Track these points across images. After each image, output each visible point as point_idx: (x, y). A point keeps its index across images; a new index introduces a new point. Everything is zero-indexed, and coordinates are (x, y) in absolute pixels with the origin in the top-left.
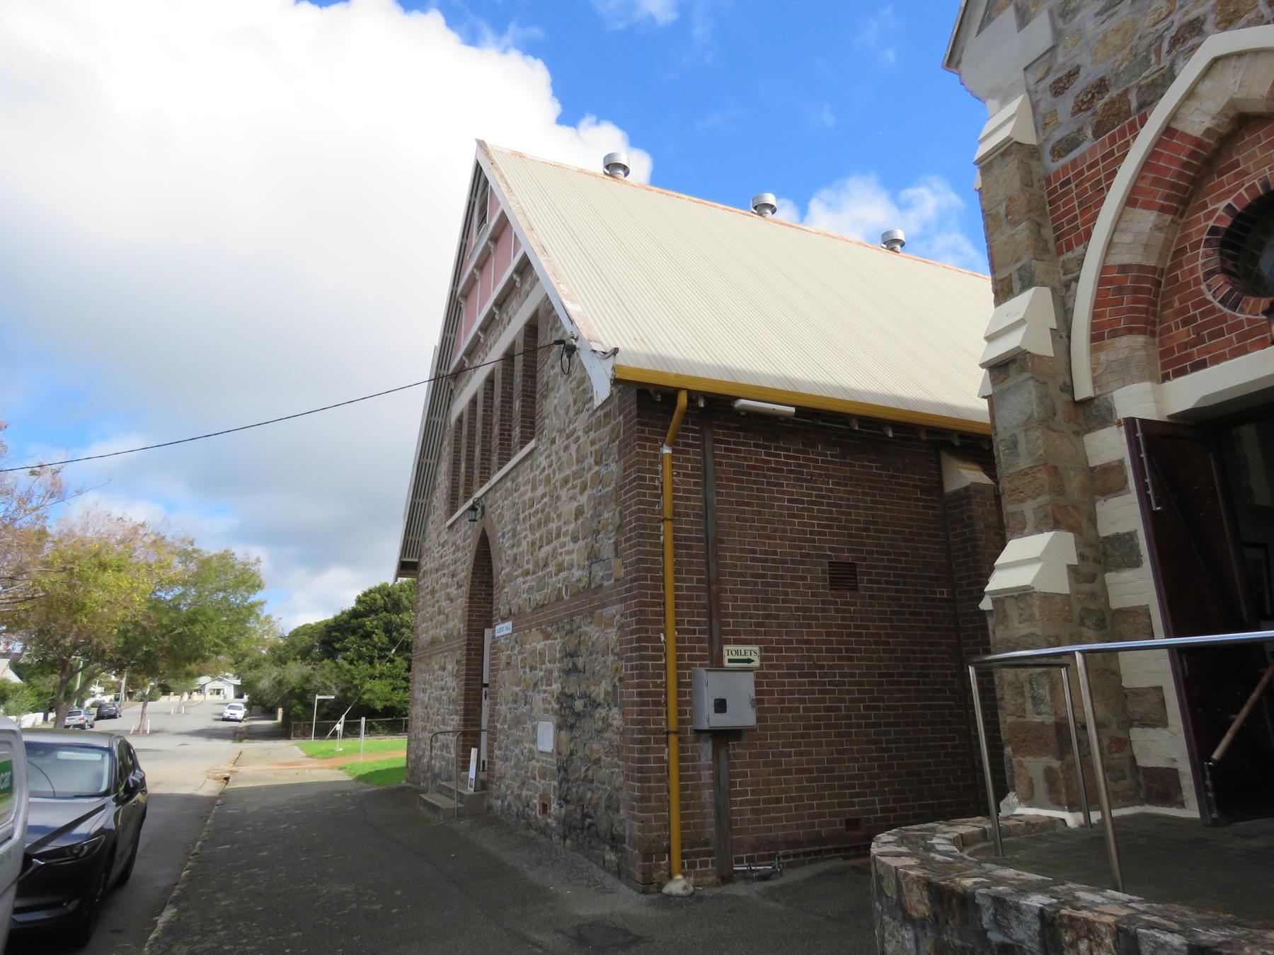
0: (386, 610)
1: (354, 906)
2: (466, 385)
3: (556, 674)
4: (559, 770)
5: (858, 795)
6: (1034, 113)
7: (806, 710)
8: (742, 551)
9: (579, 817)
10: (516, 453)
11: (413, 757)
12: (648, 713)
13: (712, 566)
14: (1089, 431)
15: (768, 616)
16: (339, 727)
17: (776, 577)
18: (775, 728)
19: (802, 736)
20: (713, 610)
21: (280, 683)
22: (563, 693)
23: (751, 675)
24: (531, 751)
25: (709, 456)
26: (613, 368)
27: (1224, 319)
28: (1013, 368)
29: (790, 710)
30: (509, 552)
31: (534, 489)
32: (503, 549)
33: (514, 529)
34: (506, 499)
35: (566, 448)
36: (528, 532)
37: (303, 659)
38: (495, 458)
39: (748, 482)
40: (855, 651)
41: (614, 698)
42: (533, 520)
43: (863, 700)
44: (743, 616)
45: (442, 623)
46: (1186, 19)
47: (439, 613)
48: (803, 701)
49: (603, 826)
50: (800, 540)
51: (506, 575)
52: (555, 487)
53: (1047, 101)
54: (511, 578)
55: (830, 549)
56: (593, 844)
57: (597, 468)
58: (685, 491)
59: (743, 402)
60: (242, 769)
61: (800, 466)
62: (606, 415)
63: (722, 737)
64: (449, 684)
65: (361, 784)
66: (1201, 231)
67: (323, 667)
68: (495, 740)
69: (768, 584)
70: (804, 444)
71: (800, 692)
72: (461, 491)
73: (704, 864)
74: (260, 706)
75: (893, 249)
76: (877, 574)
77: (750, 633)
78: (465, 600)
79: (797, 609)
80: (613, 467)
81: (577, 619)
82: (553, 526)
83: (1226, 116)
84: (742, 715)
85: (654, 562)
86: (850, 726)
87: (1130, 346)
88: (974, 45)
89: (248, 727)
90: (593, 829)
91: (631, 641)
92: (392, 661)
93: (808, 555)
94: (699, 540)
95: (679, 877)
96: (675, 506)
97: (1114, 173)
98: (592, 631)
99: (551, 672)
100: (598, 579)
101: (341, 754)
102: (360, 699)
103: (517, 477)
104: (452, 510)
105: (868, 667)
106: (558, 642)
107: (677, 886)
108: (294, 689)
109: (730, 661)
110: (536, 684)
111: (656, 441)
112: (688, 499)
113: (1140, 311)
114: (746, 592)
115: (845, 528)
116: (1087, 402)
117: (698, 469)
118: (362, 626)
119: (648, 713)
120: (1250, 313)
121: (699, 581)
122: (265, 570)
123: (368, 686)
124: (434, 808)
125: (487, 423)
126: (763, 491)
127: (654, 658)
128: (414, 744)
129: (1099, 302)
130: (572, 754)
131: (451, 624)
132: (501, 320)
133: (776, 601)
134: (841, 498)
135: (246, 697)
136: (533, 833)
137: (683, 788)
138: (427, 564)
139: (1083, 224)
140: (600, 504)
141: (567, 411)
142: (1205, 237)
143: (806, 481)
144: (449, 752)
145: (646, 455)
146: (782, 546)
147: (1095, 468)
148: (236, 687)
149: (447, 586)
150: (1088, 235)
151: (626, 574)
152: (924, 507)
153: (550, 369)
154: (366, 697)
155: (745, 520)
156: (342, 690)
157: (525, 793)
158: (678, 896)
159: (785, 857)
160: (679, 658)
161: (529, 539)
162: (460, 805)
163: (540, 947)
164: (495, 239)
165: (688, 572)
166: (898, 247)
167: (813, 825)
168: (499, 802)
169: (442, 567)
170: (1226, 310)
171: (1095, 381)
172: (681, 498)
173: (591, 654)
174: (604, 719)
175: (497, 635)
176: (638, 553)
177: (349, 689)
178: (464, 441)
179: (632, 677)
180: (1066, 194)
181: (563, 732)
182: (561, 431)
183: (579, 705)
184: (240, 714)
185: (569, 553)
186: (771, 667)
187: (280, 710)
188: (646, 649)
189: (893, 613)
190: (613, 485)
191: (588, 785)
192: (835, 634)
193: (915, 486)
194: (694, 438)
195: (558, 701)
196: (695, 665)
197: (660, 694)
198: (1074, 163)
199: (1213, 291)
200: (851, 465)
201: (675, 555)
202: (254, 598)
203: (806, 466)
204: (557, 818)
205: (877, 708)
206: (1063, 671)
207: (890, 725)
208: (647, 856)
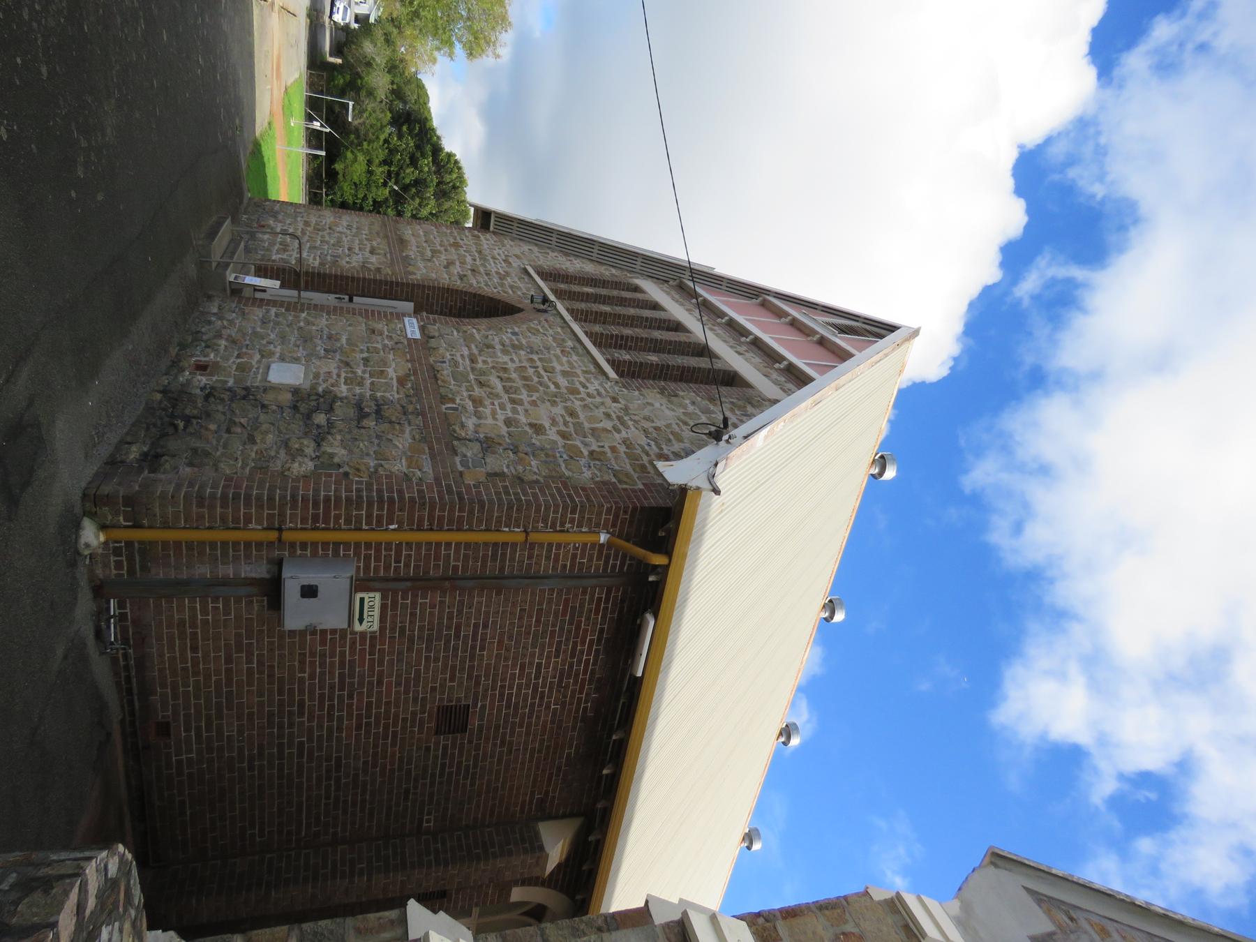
0: (439, 183)
1: (84, 144)
2: (673, 298)
3: (358, 390)
4: (246, 389)
5: (198, 735)
7: (302, 680)
8: (487, 613)
9: (187, 412)
10: (603, 354)
11: (277, 208)
12: (305, 508)
13: (471, 583)
15: (411, 640)
16: (316, 125)
17: (456, 649)
18: (281, 647)
19: (271, 676)
20: (422, 582)
21: (369, 64)
22: (335, 398)
23: (345, 626)
24: (272, 354)
25: (594, 581)
26: (698, 488)
29: (302, 663)
30: (497, 339)
31: (565, 374)
32: (498, 333)
33: (520, 347)
34: (554, 339)
35: (608, 416)
36: (518, 364)
37: (393, 92)
38: (597, 328)
39: (563, 621)
40: (368, 732)
41: (325, 463)
42: (531, 371)
43: (310, 740)
44: (413, 615)
45: (422, 254)
47: (433, 252)
48: (312, 677)
49: (172, 444)
50: (495, 675)
51: (472, 335)
52: (566, 400)
54: (468, 339)
55: (483, 707)
56: (153, 430)
57: (586, 453)
58: (557, 555)
59: (652, 623)
60: (275, 15)
61: (577, 675)
62: (643, 467)
63: (273, 590)
64: (355, 258)
65: (250, 147)
67: (383, 111)
68: (288, 310)
69: (448, 642)
70: (599, 680)
71: (322, 674)
72: (562, 286)
73: (119, 565)
74: (346, 39)
75: (781, 734)
76: (453, 754)
77: (393, 622)
78: (447, 282)
79: (418, 672)
80: (587, 474)
81: (419, 421)
82: (524, 395)
84: (297, 614)
85: (480, 521)
86: (281, 727)
88: (1013, 882)
89: (323, 26)
90: (171, 430)
91: (390, 490)
92: (385, 184)
93: (478, 683)
94: (502, 569)
95: (102, 538)
96: (541, 545)
98: (404, 440)
99: (361, 384)
100: (464, 450)
101: (287, 123)
102: (347, 148)
103: (577, 354)
104: (545, 275)
105: (348, 745)
106: (394, 395)
107: (91, 536)
108: (361, 78)
109: (362, 600)
110: (347, 364)
111: (614, 525)
112: (548, 558)
114: (441, 618)
115: (506, 722)
117: (580, 569)
118: (423, 155)
119: (305, 508)
121: (455, 568)
122: (487, 60)
123: (361, 157)
124: (213, 234)
125: (632, 321)
126: (552, 637)
127: (369, 516)
128: (291, 210)
130: (264, 406)
131: (421, 264)
132: (741, 344)
133: (428, 649)
134: (538, 717)
135: (356, 26)
136: (174, 351)
137: (213, 545)
138: (487, 240)
140: (547, 455)
141: (647, 419)
143: (561, 681)
144: (278, 253)
145: (599, 514)
146: (490, 657)
148: (368, 16)
149: (463, 263)
151: (468, 487)
152: (524, 802)
153: (691, 403)
154: (349, 155)
155: (521, 618)
156: (357, 130)
157: (223, 343)
158: (78, 537)
159: (125, 656)
160: (368, 545)
161: (511, 366)
162: (214, 265)
163: (7, 381)
164: (822, 342)
165: (466, 556)
166: (783, 739)
167: (163, 686)
168: (215, 310)
169: (483, 258)
172: (549, 550)
173: (378, 437)
174: (300, 451)
175: (406, 319)
176: (491, 502)
177: (358, 137)
178: (615, 293)
179: (349, 490)
181: (289, 396)
182: (626, 409)
183: (320, 419)
184: (338, 17)
185: (494, 413)
186: (353, 643)
187: (339, 61)
188: (381, 508)
189: (409, 772)
190: (567, 473)
191: (224, 427)
192: (387, 711)
193: (547, 793)
194: (614, 566)
195: (327, 392)
196: (359, 561)
197: (326, 521)
200: (574, 728)
201: (486, 544)
202: (458, 48)
203: (576, 682)
204: (189, 382)
205: (301, 755)
207: (281, 769)
208: (129, 501)
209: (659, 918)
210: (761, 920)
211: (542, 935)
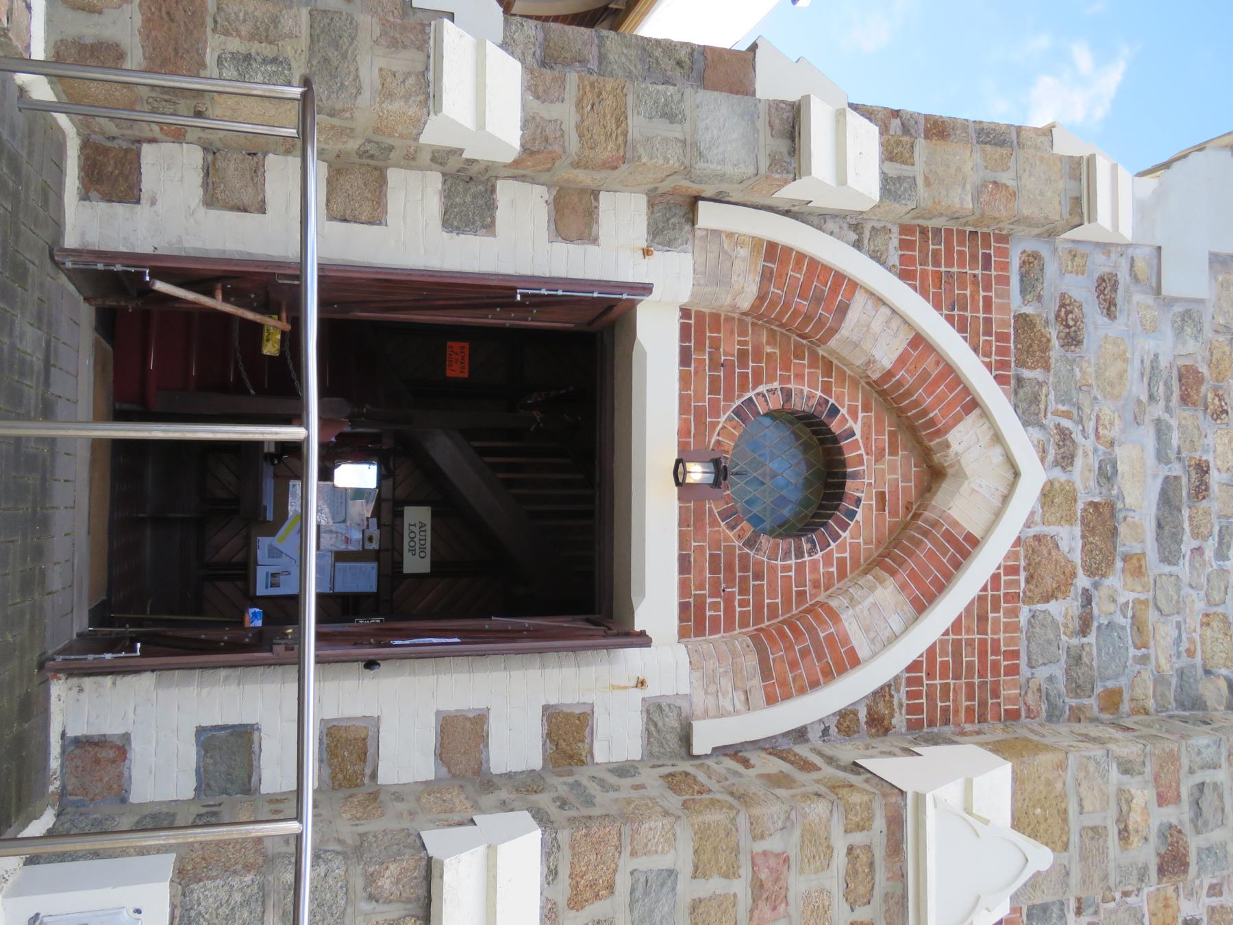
6: (1097, 244)
14: (651, 205)
27: (729, 397)
28: (783, 146)
46: (1080, 452)
53: (1100, 264)
66: (840, 398)
83: (951, 466)
87: (744, 290)
97: (962, 329)
113: (782, 313)
116: (691, 216)
120: (724, 428)
129: (815, 267)
139: (924, 272)
142: (832, 401)
147: (597, 199)
150: (905, 276)
170: (738, 403)
171: (716, 233)
180: (974, 257)
198: (1004, 281)
199: (766, 394)
206: (292, 132)
209: (770, 85)
210: (896, 123)
211: (599, 47)
